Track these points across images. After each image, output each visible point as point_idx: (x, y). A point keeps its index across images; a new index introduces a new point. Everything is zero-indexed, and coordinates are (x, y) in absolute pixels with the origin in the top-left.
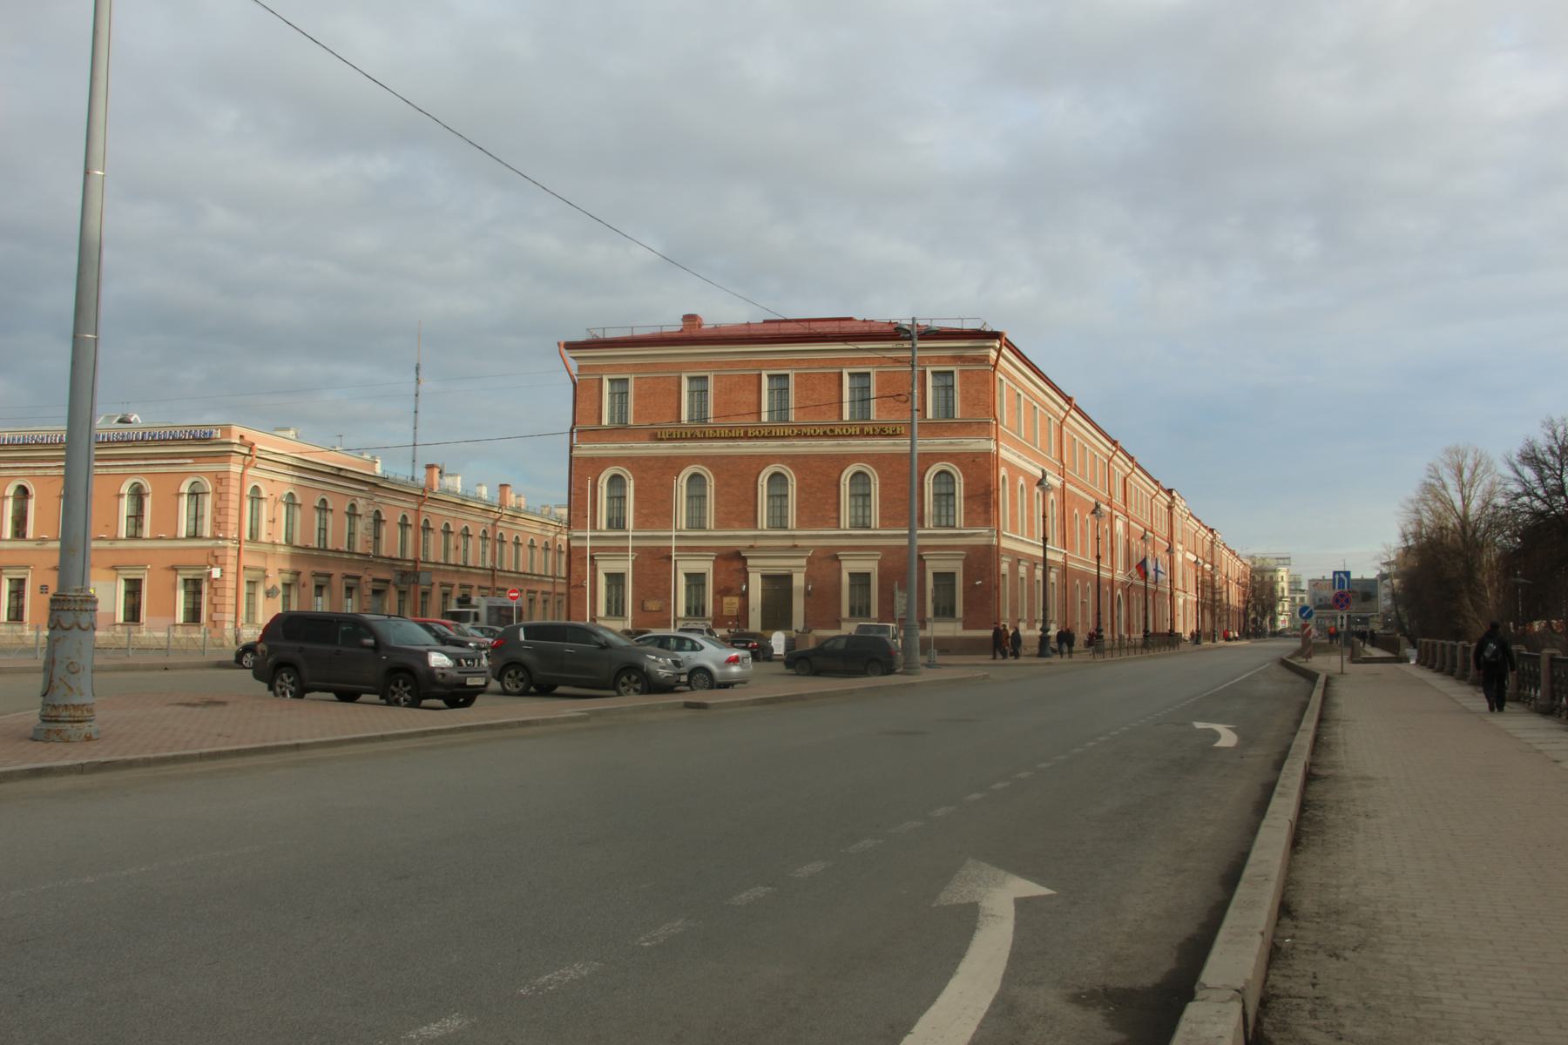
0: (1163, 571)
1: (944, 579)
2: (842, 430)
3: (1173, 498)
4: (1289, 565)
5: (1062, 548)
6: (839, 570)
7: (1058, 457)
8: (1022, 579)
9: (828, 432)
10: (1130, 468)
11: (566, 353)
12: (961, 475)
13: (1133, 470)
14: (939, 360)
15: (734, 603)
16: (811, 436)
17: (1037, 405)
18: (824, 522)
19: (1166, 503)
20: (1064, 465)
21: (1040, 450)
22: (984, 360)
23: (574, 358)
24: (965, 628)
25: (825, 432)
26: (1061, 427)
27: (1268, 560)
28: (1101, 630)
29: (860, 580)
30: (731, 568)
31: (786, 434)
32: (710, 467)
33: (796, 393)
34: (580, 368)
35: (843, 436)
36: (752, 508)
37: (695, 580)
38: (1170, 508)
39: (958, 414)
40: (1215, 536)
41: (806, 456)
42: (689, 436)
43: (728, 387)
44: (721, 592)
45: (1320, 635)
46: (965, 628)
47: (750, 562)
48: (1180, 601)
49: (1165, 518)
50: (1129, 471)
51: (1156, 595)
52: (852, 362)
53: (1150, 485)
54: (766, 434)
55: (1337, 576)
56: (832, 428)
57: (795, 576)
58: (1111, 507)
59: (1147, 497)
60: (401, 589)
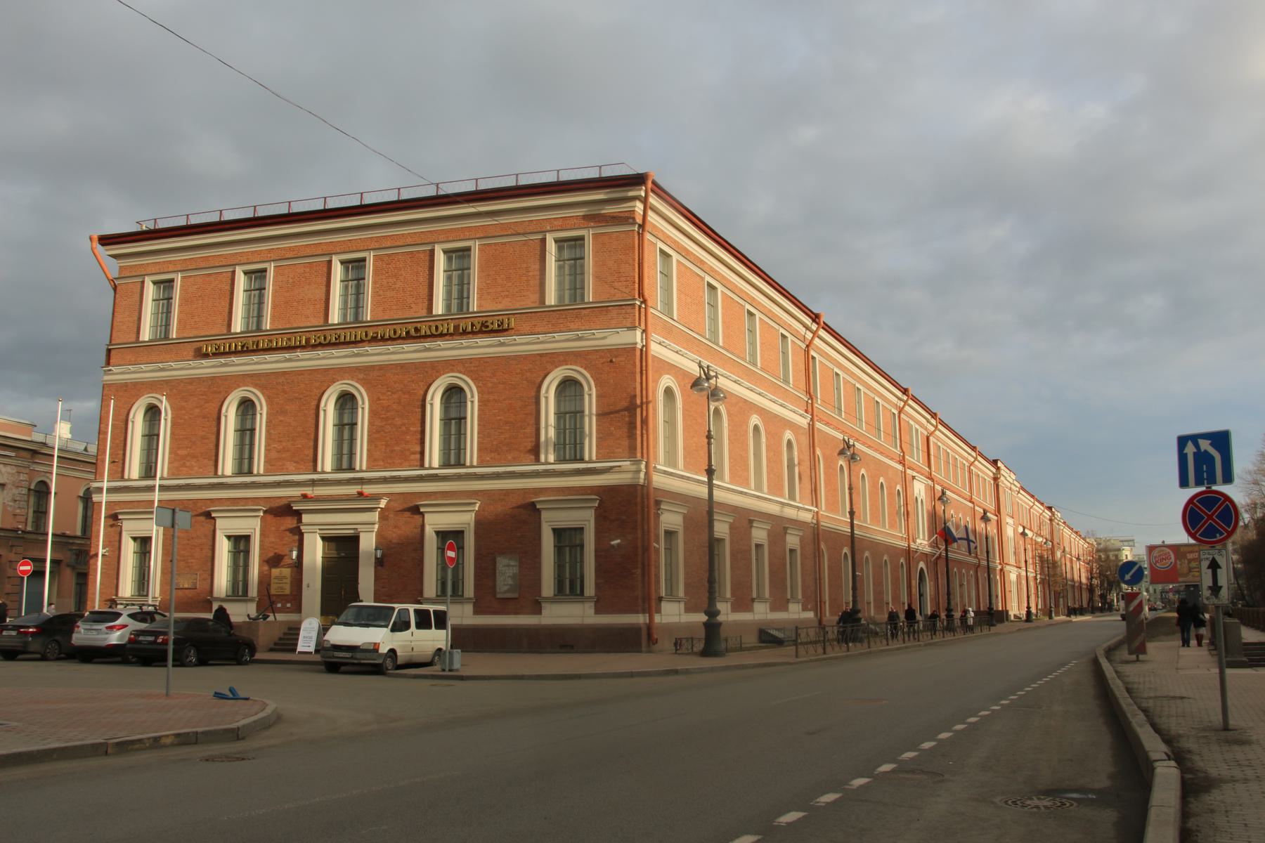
0: (974, 540)
1: (567, 538)
3: (998, 469)
4: (1134, 546)
5: (812, 505)
7: (803, 385)
8: (758, 546)
9: (413, 333)
10: (932, 425)
11: (100, 250)
12: (593, 383)
13: (936, 427)
14: (564, 224)
15: (285, 577)
16: (391, 339)
17: (839, 372)
18: (401, 459)
19: (1048, 517)
20: (904, 453)
21: (762, 369)
22: (628, 219)
23: (115, 256)
24: (598, 611)
27: (1112, 541)
28: (952, 610)
29: (450, 537)
30: (283, 528)
31: (358, 339)
32: (262, 388)
33: (374, 282)
35: (432, 336)
36: (312, 443)
37: (240, 543)
39: (590, 296)
40: (1053, 514)
41: (382, 368)
43: (291, 280)
44: (273, 561)
45: (1164, 608)
48: (1013, 577)
49: (990, 489)
50: (932, 429)
51: (979, 569)
52: (447, 236)
53: (968, 453)
55: (1190, 449)
56: (419, 326)
57: (362, 535)
58: (904, 465)
59: (1026, 508)
60: (80, 571)
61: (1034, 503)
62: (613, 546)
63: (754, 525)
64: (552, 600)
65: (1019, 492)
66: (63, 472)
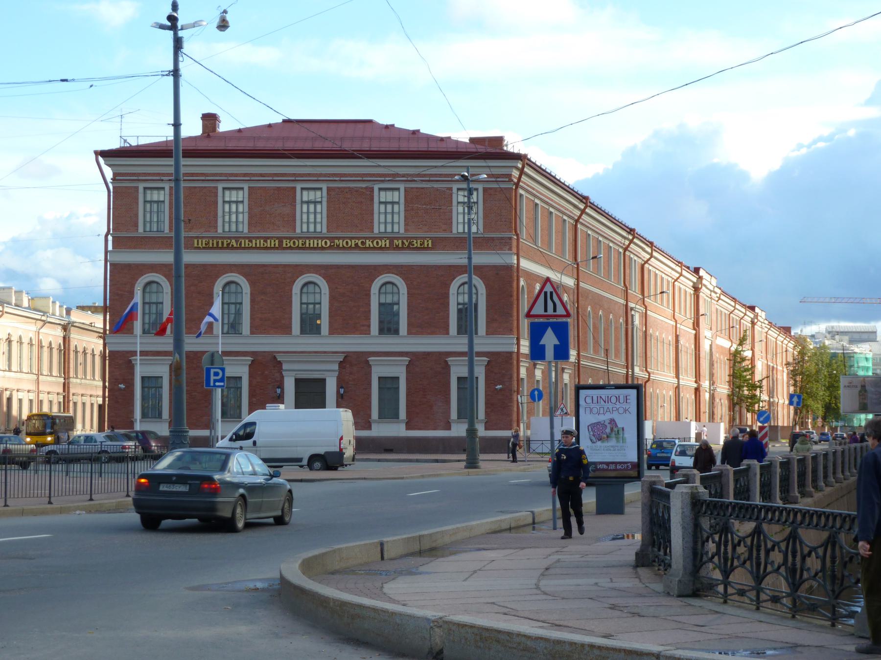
2: (372, 242)
3: (700, 278)
6: (369, 374)
8: (538, 381)
9: (360, 244)
24: (408, 428)
25: (356, 245)
26: (576, 226)
32: (245, 275)
34: (115, 175)
38: (696, 289)
42: (225, 245)
46: (408, 428)
47: (285, 367)
49: (690, 301)
54: (300, 246)
59: (668, 282)
61: (734, 307)
62: (497, 389)
63: (537, 367)
64: (375, 421)
65: (719, 299)
66: (144, 341)
